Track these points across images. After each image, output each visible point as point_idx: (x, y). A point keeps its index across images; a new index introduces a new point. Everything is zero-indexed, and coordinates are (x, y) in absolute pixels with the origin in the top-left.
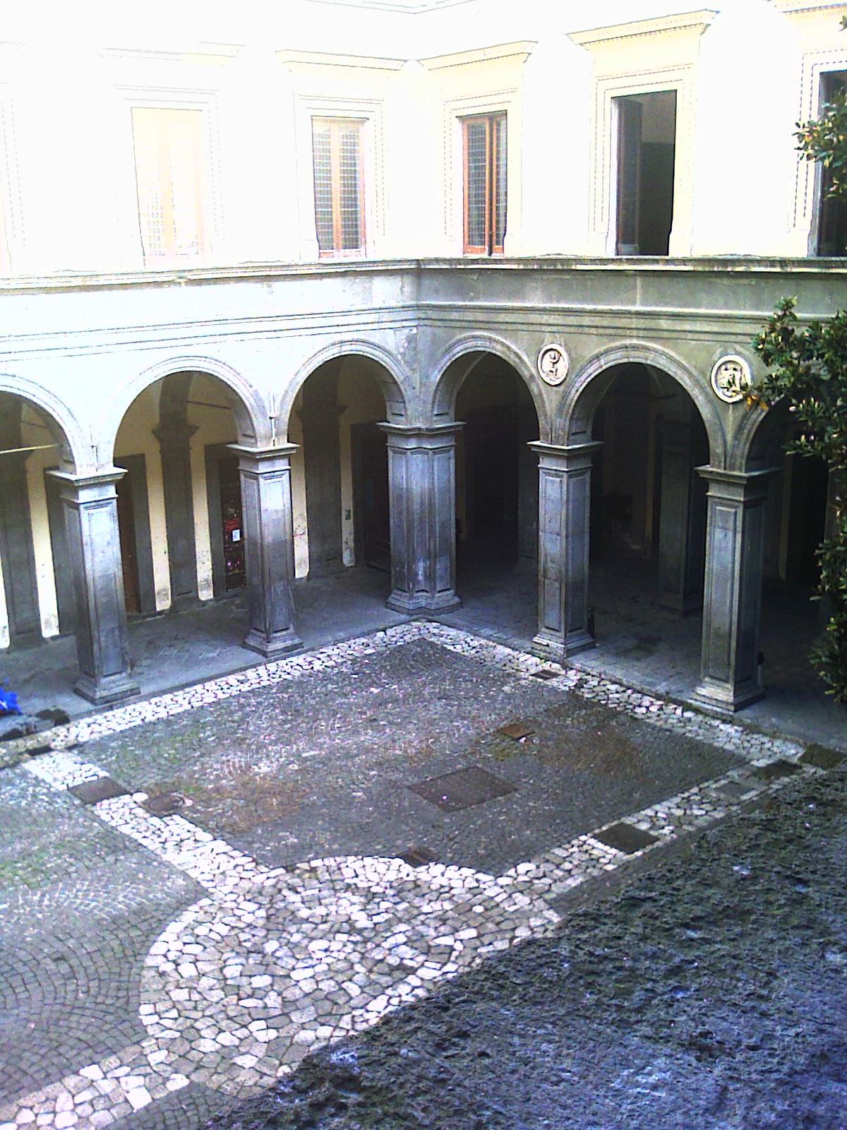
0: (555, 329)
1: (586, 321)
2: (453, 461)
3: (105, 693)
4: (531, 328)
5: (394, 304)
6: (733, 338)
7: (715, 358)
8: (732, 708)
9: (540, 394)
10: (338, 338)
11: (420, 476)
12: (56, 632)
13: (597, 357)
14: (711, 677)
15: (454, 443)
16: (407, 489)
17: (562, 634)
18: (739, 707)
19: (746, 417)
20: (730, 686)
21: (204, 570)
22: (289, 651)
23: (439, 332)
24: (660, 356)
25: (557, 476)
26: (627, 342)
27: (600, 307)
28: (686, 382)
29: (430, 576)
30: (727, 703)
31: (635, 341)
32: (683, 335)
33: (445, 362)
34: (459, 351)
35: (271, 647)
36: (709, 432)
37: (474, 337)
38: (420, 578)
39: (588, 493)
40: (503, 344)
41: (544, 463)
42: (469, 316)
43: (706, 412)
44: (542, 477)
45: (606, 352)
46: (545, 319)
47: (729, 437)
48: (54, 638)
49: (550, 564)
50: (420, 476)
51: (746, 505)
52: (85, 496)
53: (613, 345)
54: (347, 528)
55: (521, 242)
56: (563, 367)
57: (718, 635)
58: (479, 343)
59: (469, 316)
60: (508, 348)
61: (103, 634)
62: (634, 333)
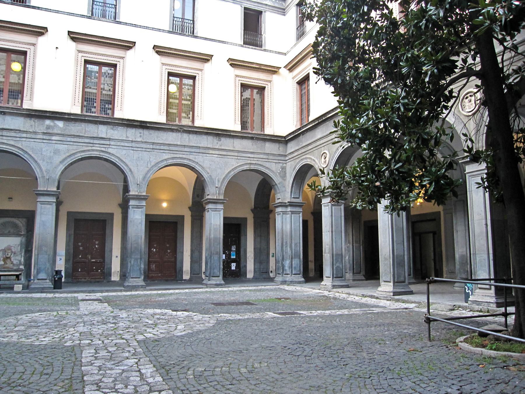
3: (130, 284)
8: (392, 294)
10: (249, 162)
18: (395, 294)
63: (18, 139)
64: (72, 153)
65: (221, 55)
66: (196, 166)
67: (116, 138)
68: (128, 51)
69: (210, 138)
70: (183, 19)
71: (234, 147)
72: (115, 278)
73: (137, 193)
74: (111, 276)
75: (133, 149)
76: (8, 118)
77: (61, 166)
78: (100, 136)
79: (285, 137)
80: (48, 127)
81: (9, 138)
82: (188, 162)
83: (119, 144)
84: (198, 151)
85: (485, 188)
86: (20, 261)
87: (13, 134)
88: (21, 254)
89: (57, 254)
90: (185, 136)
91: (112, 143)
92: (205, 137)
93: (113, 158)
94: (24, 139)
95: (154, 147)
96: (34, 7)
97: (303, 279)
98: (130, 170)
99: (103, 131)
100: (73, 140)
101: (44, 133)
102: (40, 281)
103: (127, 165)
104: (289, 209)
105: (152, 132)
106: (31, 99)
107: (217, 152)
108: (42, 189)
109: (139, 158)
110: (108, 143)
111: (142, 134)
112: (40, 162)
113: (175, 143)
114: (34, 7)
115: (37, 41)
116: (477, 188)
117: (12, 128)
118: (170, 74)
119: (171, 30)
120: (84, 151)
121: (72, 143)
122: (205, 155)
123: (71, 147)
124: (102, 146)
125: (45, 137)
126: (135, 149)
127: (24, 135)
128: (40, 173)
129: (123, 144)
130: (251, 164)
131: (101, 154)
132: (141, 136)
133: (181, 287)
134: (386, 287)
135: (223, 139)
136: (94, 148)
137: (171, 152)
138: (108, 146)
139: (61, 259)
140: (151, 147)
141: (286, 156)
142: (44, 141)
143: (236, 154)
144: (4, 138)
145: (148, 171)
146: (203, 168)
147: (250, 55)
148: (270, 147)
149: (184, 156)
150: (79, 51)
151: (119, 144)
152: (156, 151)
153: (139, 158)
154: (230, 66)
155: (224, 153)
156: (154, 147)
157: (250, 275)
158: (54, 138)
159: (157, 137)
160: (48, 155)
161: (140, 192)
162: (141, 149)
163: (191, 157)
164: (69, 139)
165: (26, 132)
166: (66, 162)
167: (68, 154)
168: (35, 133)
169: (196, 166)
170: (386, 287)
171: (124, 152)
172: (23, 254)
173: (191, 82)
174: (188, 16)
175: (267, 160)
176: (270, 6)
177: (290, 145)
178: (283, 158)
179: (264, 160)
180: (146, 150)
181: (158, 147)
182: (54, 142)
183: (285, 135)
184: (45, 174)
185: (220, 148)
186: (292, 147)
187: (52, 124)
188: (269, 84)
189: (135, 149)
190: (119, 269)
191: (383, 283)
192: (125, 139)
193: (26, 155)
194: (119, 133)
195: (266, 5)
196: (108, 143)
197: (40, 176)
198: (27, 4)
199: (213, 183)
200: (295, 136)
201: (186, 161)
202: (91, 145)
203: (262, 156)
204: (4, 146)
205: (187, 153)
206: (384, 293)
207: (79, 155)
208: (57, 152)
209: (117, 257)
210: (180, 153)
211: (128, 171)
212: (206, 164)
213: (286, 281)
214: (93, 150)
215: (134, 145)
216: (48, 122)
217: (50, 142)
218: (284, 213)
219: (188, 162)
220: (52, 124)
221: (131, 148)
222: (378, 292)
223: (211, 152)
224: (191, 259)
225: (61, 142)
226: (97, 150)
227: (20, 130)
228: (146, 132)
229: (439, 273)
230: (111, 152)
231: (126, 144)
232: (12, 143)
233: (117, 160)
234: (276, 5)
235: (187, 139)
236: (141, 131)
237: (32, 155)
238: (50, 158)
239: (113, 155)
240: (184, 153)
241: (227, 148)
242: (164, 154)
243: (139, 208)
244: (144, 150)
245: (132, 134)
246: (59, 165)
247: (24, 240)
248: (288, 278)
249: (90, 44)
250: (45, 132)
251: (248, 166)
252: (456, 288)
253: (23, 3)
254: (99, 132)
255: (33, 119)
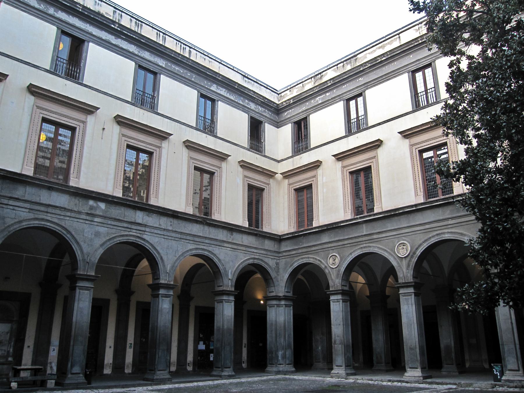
0: (333, 248)
1: (346, 242)
2: (292, 311)
3: (158, 377)
4: (324, 250)
5: (272, 249)
6: (401, 235)
7: (395, 243)
8: (422, 378)
9: (329, 272)
10: (253, 256)
11: (280, 316)
12: (130, 372)
13: (351, 254)
14: (410, 368)
15: (292, 304)
16: (276, 321)
17: (344, 367)
18: (425, 378)
19: (410, 261)
20: (419, 370)
21: (190, 358)
22: (230, 377)
23: (288, 260)
24: (374, 248)
25: (338, 302)
26: (362, 246)
27: (351, 236)
28: (386, 255)
29: (284, 357)
30: (419, 377)
31: (365, 245)
32: (383, 239)
33: (290, 270)
34: (296, 265)
35: (223, 374)
36: (397, 270)
37: (302, 258)
38: (280, 358)
39: (349, 310)
40: (313, 258)
41: (332, 298)
42: (300, 251)
43: (394, 263)
44: (331, 303)
45: (354, 251)
46: (330, 245)
47: (405, 270)
48: (129, 374)
49: (337, 338)
50: (280, 316)
51: (416, 295)
52: (162, 292)
53: (357, 248)
54: (245, 351)
55: (322, 217)
56: (337, 261)
57: (411, 349)
58: (304, 260)
59: (300, 251)
60: (316, 259)
61: (161, 351)
62: (364, 242)
63: (62, 217)
64: (111, 237)
65: (108, 109)
66: (214, 258)
67: (151, 225)
68: (163, 142)
69: (225, 232)
70: (144, 92)
71: (242, 242)
72: (107, 371)
73: (166, 282)
74: (103, 369)
75: (164, 237)
76: (54, 194)
77: (101, 249)
78: (137, 221)
79: (280, 236)
80: (92, 208)
81: (53, 216)
82: (207, 253)
83: (153, 231)
84: (216, 243)
85: (510, 307)
86: (8, 352)
87: (58, 211)
88: (10, 343)
89: (51, 344)
90: (206, 228)
91: (147, 230)
92: (221, 230)
93: (147, 244)
94: (68, 218)
95: (182, 237)
96: (86, 86)
97: (294, 369)
98: (161, 258)
99: (140, 217)
100: (113, 223)
101: (88, 214)
102: (73, 376)
103: (158, 253)
104: (283, 302)
105: (180, 222)
106: (78, 177)
107: (230, 246)
108: (82, 273)
109: (168, 246)
110: (143, 229)
111: (172, 223)
112: (82, 243)
113: (199, 234)
114: (86, 86)
115: (86, 119)
116: (504, 306)
117: (57, 205)
118: (45, 120)
119: (52, 71)
120: (123, 236)
121: (112, 227)
122: (221, 248)
123: (114, 231)
124: (138, 232)
125: (88, 218)
126: (166, 237)
127: (69, 214)
128: (80, 255)
129: (156, 231)
130: (254, 258)
131: (137, 240)
132: (171, 225)
133: (188, 380)
134: (413, 373)
135: (234, 234)
136: (131, 233)
137: (195, 243)
138: (143, 233)
139: (54, 350)
140: (179, 236)
141: (279, 253)
142: (87, 222)
143: (244, 249)
144: (49, 215)
145: (176, 260)
146: (219, 260)
147: (253, 158)
148: (269, 245)
149: (205, 248)
150: (124, 135)
151: (153, 231)
152: (183, 240)
153: (168, 246)
154: (239, 167)
155: (184, 236)
156: (182, 237)
157: (128, 370)
158: (96, 219)
159: (185, 227)
160: (90, 237)
161: (170, 281)
162: (171, 238)
163: (210, 249)
164: (109, 222)
165: (71, 211)
166: (105, 245)
167: (108, 238)
168: (79, 213)
169: (214, 258)
170: (413, 373)
171: (157, 239)
172: (12, 343)
173: (69, 133)
174: (149, 90)
175: (266, 256)
176: (268, 118)
177: (283, 244)
178: (277, 255)
179: (264, 255)
180: (175, 239)
181: (184, 237)
182: (96, 224)
183: (280, 234)
184: (86, 257)
185: (232, 242)
186: (286, 247)
187: (95, 205)
188: (158, 150)
189: (166, 237)
190: (111, 361)
191: (409, 369)
192: (158, 226)
193: (68, 235)
194: (152, 220)
195: (266, 117)
196: (143, 229)
197: (81, 258)
198: (80, 81)
199: (227, 275)
200: (292, 237)
201: (206, 253)
202: (129, 230)
203: (262, 252)
204: (48, 224)
205: (207, 245)
206: (413, 378)
207: (118, 239)
208: (97, 234)
209: (110, 347)
210: (201, 244)
211: (159, 259)
212: (221, 257)
213: (280, 371)
214: (131, 236)
215: (165, 233)
216: (91, 202)
217: (92, 223)
218: (278, 306)
219: (207, 253)
220: (95, 205)
221: (162, 236)
222: (406, 378)
223: (226, 245)
224: (178, 349)
225: (102, 225)
226: (134, 236)
227: (65, 209)
228: (175, 221)
229: (312, 365)
230: (147, 239)
231: (159, 232)
232: (56, 221)
233: (151, 247)
234: (272, 118)
235: (208, 232)
236: (171, 220)
237: (75, 236)
238: (91, 240)
239: (147, 242)
240: (205, 244)
241: (237, 242)
242: (189, 245)
243: (167, 297)
244: (173, 238)
245: (164, 222)
246: (99, 248)
247: (15, 326)
248: (281, 368)
249: (132, 129)
250: (89, 212)
251: (252, 261)
252: (444, 373)
253: (76, 79)
254: (136, 217)
255: (77, 198)
